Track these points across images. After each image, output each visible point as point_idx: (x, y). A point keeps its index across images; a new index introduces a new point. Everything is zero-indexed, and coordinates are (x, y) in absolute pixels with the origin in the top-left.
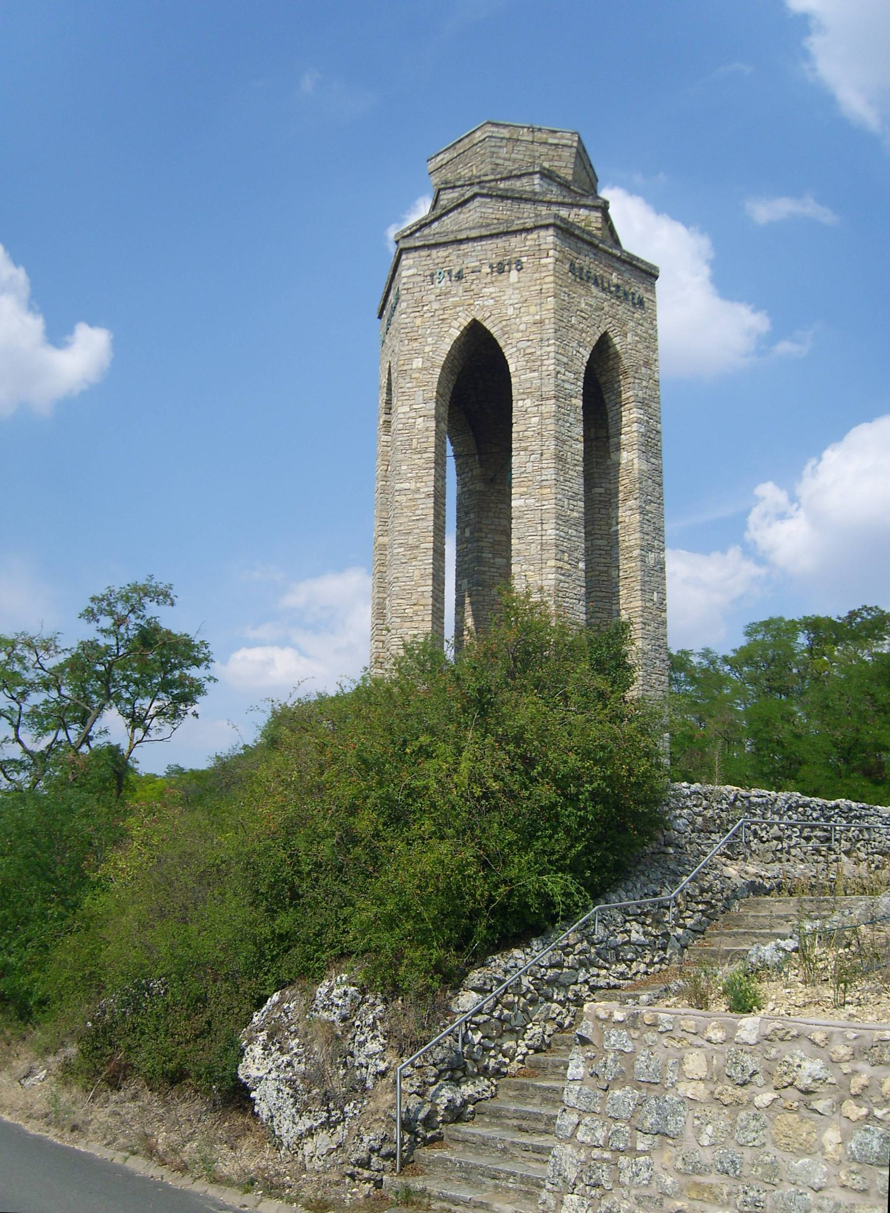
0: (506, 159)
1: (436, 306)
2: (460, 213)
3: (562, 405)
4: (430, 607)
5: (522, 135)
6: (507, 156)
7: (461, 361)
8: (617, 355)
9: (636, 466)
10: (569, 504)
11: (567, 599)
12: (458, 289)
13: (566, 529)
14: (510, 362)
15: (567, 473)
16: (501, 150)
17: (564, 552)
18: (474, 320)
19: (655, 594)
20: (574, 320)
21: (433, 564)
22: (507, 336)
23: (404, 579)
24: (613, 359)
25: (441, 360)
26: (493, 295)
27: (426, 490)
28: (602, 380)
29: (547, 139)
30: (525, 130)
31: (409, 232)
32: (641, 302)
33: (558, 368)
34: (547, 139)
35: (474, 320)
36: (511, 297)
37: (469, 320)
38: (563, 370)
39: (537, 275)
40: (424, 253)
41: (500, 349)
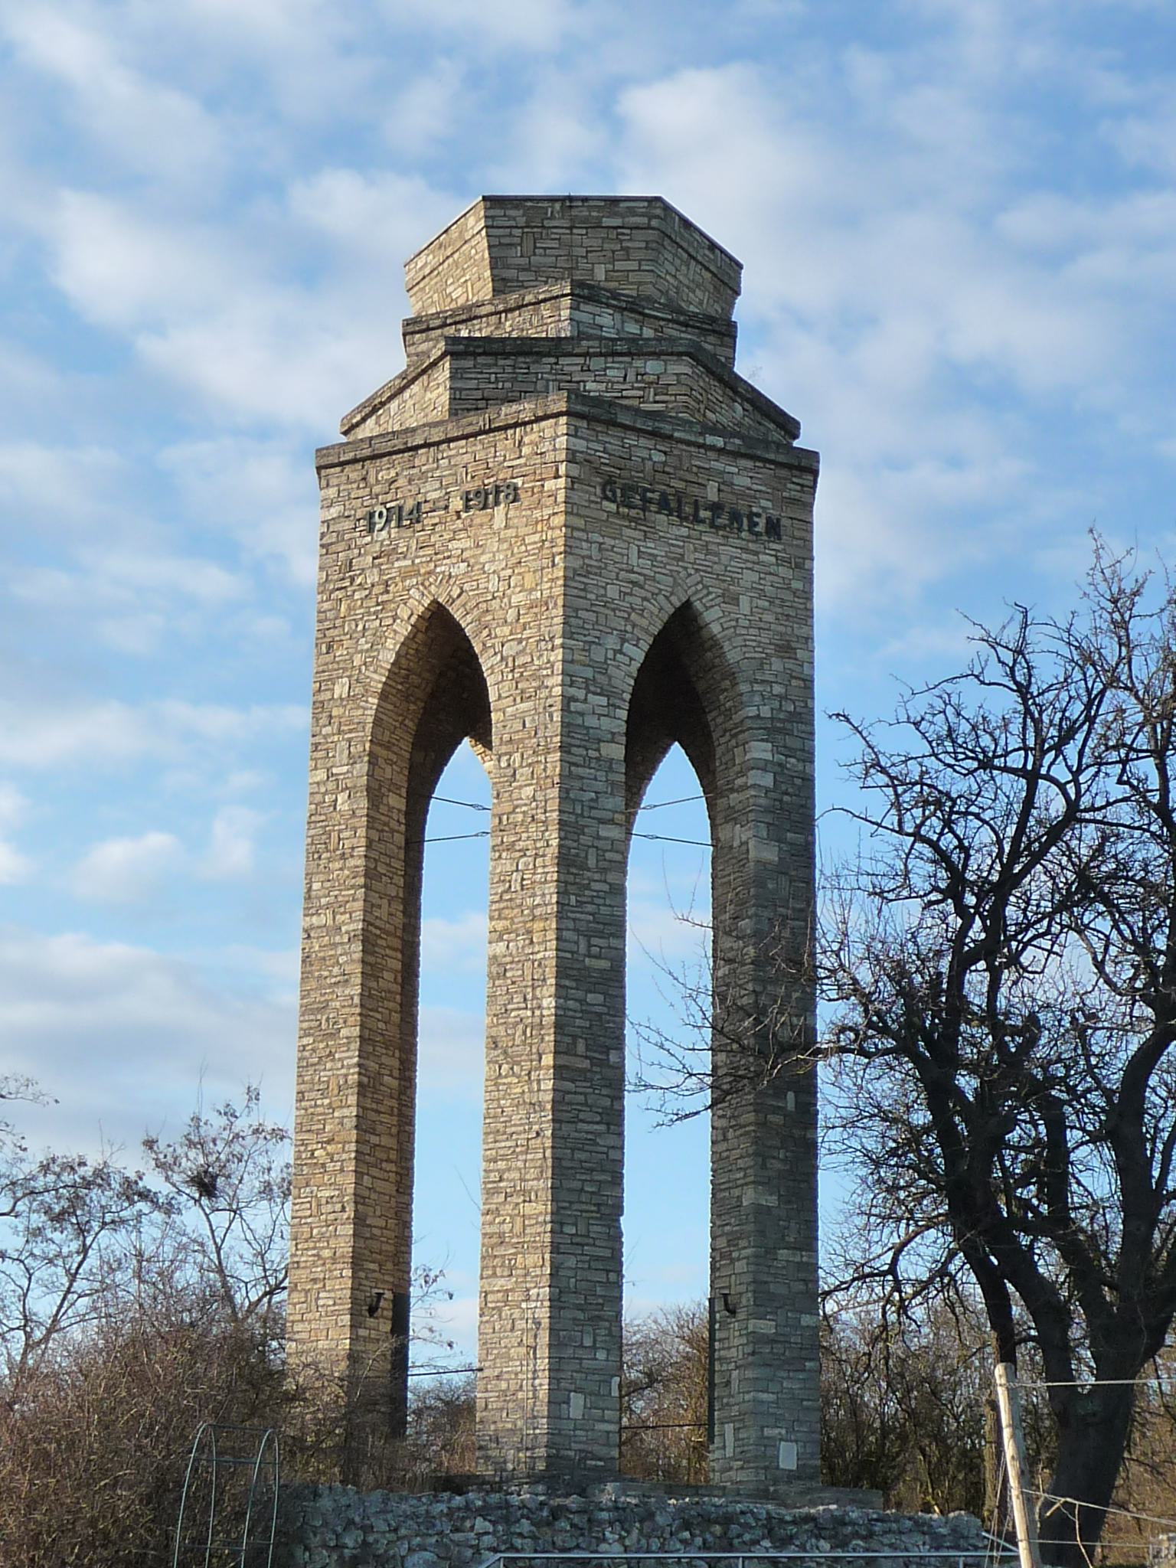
0: (522, 269)
1: (373, 577)
2: (426, 389)
3: (580, 760)
4: (353, 1147)
5: (552, 218)
6: (524, 261)
7: (427, 675)
8: (715, 644)
9: (752, 855)
10: (590, 946)
11: (580, 1125)
12: (404, 540)
13: (580, 994)
14: (490, 681)
15: (588, 887)
16: (512, 252)
17: (575, 1037)
18: (435, 602)
19: (791, 1095)
20: (612, 592)
21: (359, 1065)
22: (485, 632)
23: (313, 1095)
24: (710, 650)
25: (377, 680)
26: (466, 555)
27: (352, 927)
28: (701, 686)
29: (599, 219)
30: (558, 206)
31: (358, 418)
32: (774, 528)
33: (573, 691)
34: (599, 219)
35: (435, 602)
36: (494, 558)
37: (426, 602)
38: (580, 694)
39: (537, 514)
40: (354, 472)
41: (475, 657)
